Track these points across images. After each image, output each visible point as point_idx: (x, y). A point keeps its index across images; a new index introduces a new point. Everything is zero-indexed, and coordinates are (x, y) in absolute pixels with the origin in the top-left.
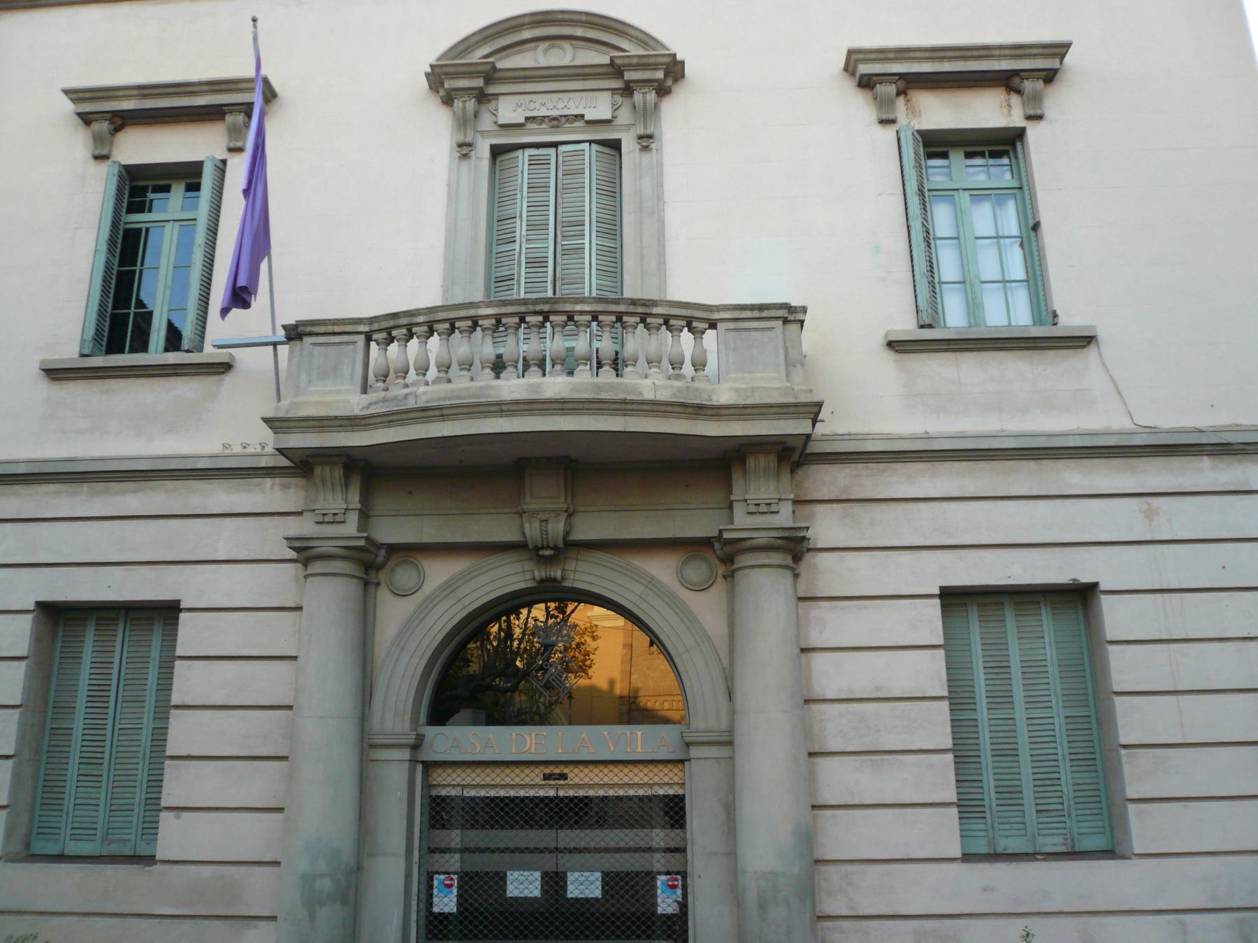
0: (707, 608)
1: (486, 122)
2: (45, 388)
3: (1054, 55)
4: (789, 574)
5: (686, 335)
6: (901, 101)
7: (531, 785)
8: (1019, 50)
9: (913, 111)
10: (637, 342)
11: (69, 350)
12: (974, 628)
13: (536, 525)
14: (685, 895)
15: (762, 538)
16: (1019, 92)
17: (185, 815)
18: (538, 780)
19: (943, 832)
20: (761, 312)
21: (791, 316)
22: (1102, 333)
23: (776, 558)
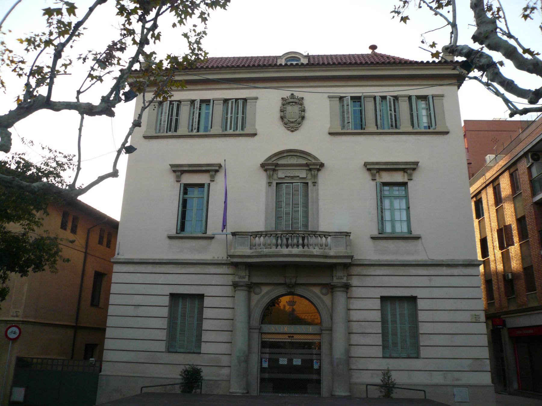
0: (327, 299)
1: (275, 177)
2: (168, 241)
6: (377, 174)
7: (285, 339)
11: (173, 232)
12: (389, 307)
14: (320, 364)
15: (339, 285)
16: (407, 172)
19: (378, 352)
20: (340, 234)
21: (348, 234)
22: (423, 236)
23: (342, 289)
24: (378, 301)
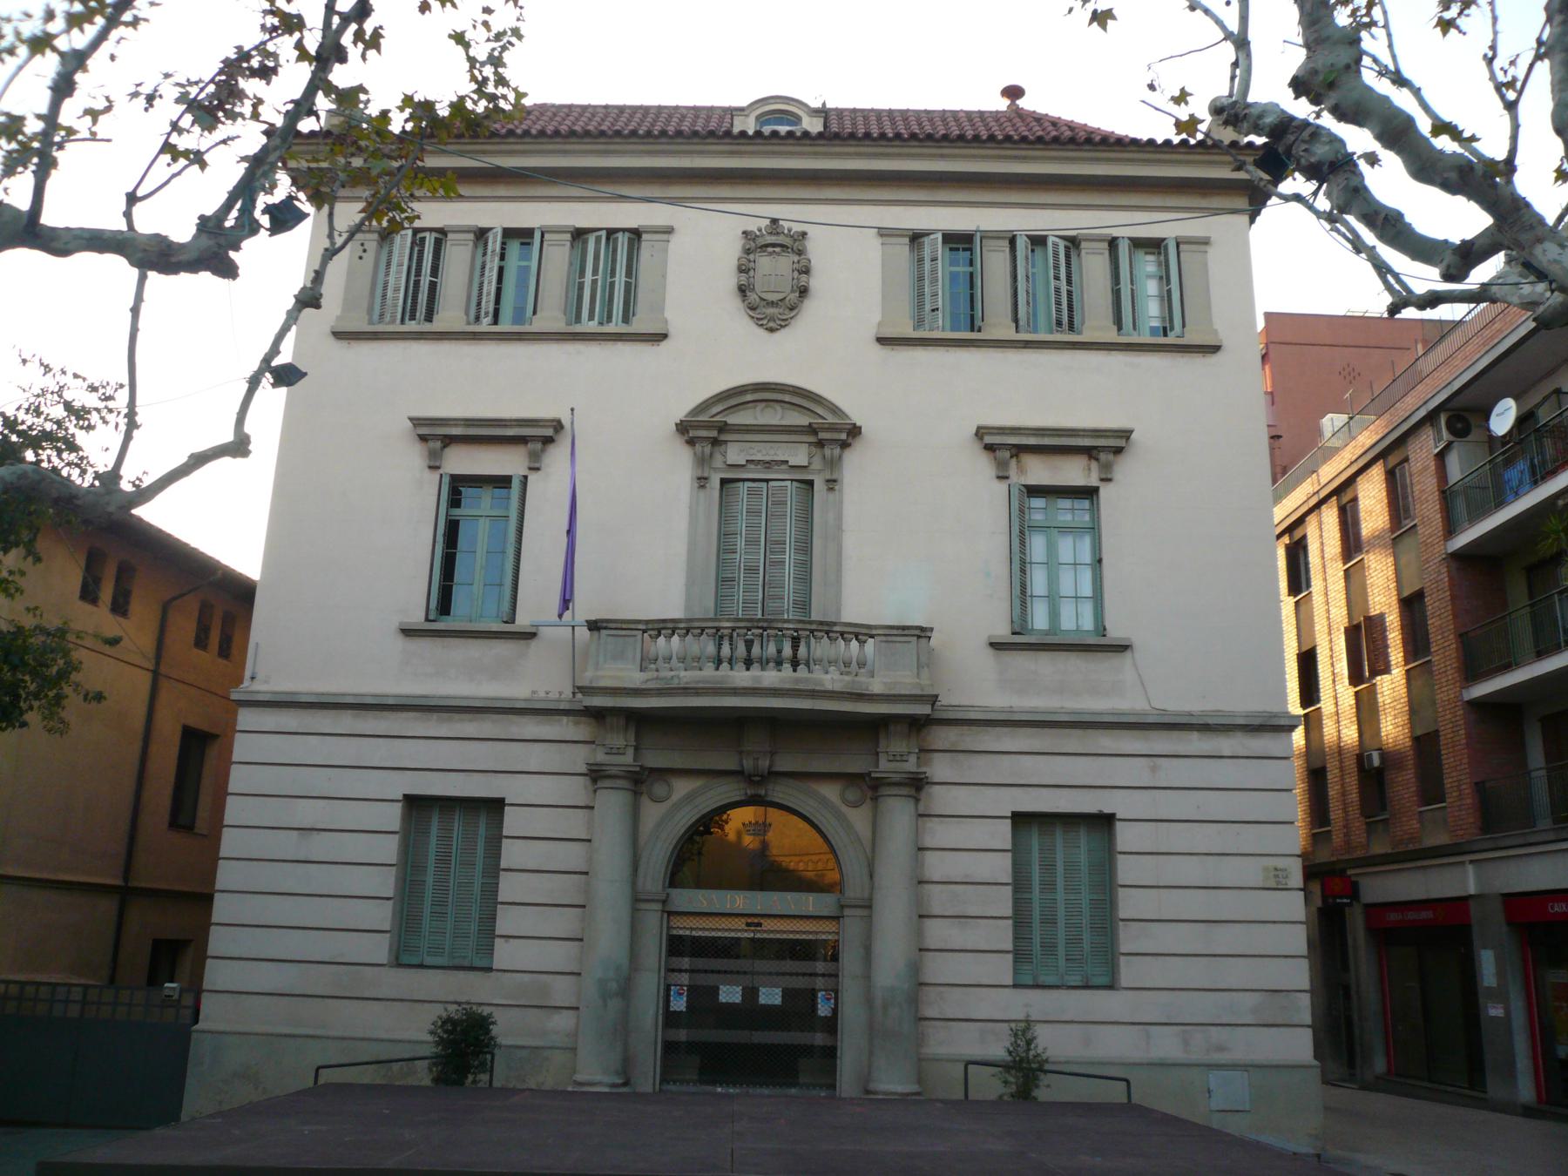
0: (859, 818)
1: (718, 462)
2: (400, 642)
4: (912, 802)
5: (854, 643)
6: (1013, 462)
10: (821, 648)
11: (417, 617)
12: (1035, 841)
14: (836, 1004)
15: (896, 777)
19: (1003, 969)
21: (923, 633)
23: (905, 791)
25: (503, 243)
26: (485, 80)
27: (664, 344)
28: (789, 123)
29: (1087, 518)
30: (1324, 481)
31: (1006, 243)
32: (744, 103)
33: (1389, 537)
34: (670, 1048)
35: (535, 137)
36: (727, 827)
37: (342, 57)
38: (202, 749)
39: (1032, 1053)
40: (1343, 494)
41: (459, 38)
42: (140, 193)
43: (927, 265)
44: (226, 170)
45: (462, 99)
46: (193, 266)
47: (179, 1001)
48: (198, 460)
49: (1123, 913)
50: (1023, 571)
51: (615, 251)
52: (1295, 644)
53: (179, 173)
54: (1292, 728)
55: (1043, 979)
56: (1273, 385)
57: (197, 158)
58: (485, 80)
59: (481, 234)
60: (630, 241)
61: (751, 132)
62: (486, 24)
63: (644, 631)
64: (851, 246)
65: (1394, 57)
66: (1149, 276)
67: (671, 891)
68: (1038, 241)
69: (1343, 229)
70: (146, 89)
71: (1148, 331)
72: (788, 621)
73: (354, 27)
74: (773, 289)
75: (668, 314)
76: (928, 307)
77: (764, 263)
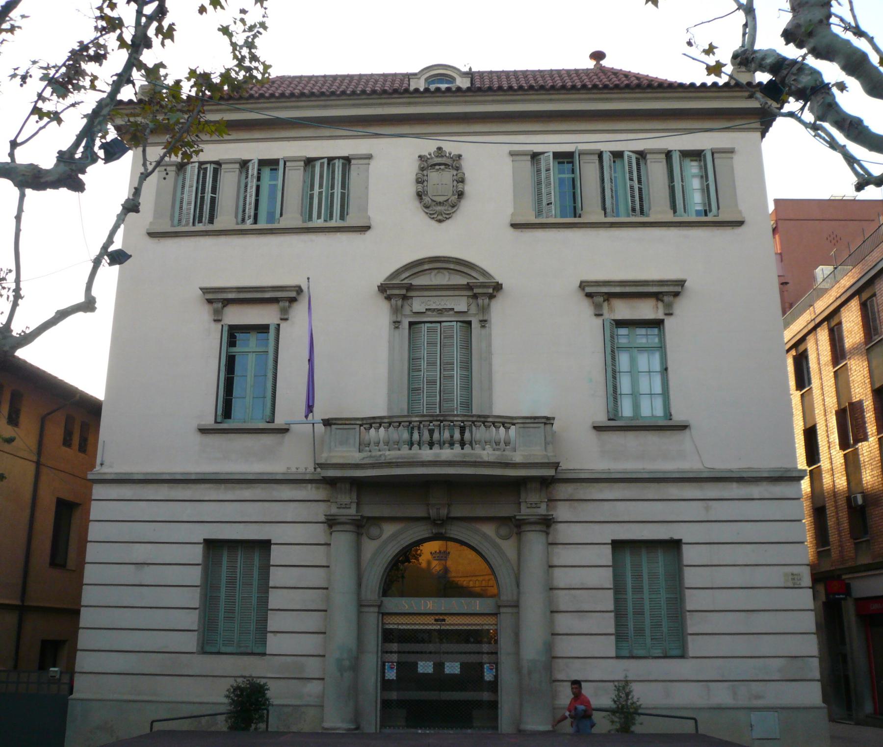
0: (508, 547)
1: (407, 310)
2: (199, 437)
3: (678, 285)
4: (544, 534)
5: (502, 429)
6: (606, 304)
7: (428, 623)
8: (662, 283)
9: (611, 309)
10: (480, 433)
11: (209, 420)
12: (628, 559)
13: (435, 510)
15: (533, 519)
16: (662, 301)
17: (278, 635)
18: (433, 622)
19: (608, 646)
21: (548, 421)
23: (538, 528)
24: (608, 550)
25: (259, 170)
26: (243, 57)
27: (368, 233)
28: (448, 82)
29: (657, 340)
30: (818, 311)
31: (596, 157)
32: (416, 70)
33: (864, 348)
34: (386, 704)
35: (278, 98)
36: (421, 559)
37: (148, 44)
38: (69, 514)
39: (630, 702)
40: (831, 321)
41: (225, 30)
42: (19, 140)
43: (543, 174)
44: (74, 122)
45: (228, 71)
46: (55, 184)
47: (60, 679)
48: (62, 315)
49: (689, 606)
50: (614, 378)
51: (333, 172)
52: (802, 423)
53: (44, 127)
54: (802, 478)
55: (636, 652)
56: (782, 248)
57: (56, 117)
58: (243, 57)
59: (244, 164)
60: (344, 166)
61: (422, 89)
62: (243, 21)
63: (361, 425)
64: (491, 164)
65: (854, 17)
66: (694, 176)
67: (384, 598)
68: (618, 155)
69: (823, 134)
70: (21, 72)
71: (694, 213)
72: (457, 416)
73: (155, 24)
74: (440, 192)
75: (370, 213)
76: (545, 202)
77: (434, 177)
